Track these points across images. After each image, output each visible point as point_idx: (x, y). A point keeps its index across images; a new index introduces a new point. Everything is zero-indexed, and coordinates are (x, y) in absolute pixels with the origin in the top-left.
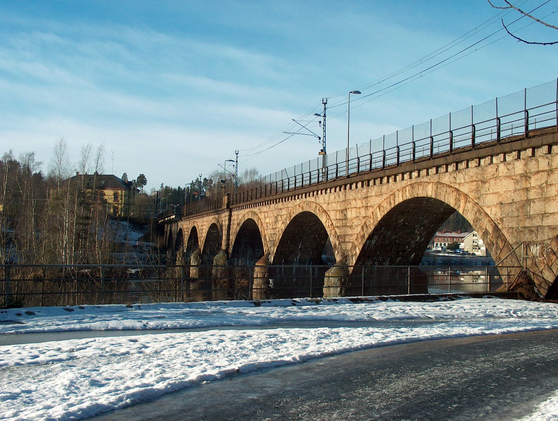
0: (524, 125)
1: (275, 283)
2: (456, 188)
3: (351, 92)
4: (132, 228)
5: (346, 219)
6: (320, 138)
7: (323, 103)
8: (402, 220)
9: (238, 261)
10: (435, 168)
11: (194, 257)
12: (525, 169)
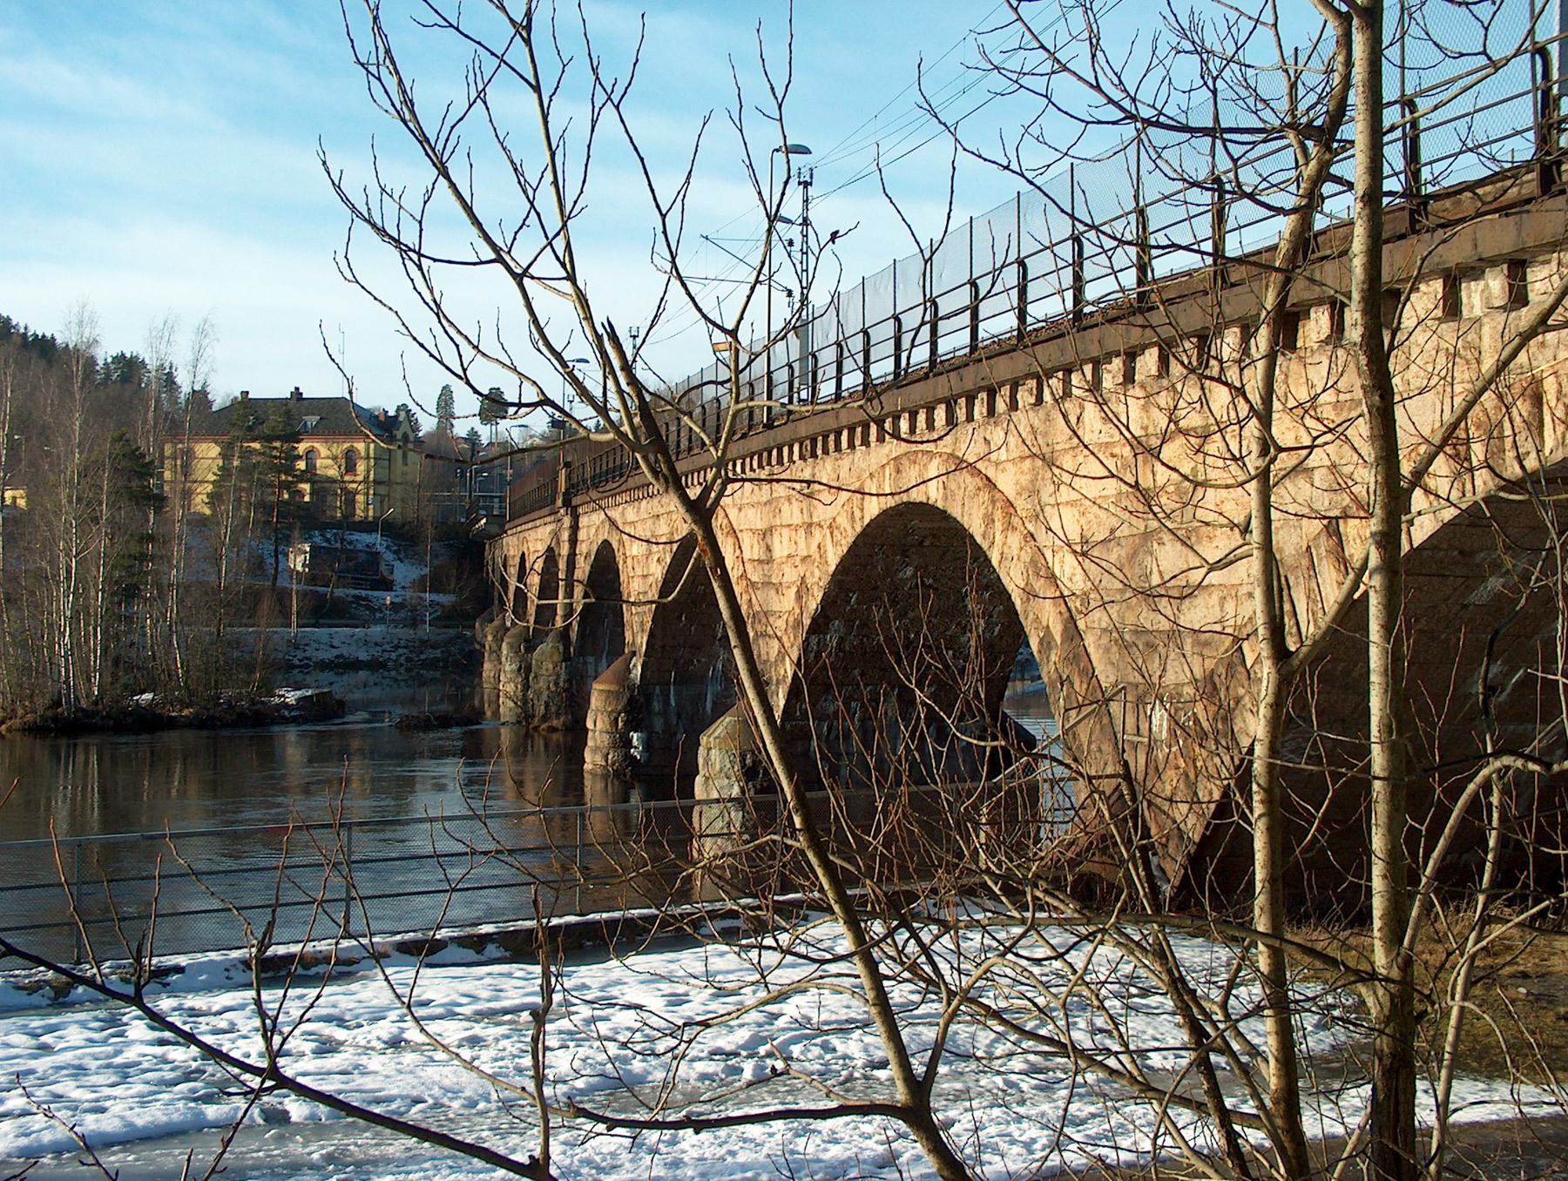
1: (648, 745)
2: (988, 478)
3: (777, 150)
4: (395, 552)
5: (770, 561)
7: (800, 183)
8: (909, 571)
9: (596, 666)
11: (511, 646)
12: (1146, 421)
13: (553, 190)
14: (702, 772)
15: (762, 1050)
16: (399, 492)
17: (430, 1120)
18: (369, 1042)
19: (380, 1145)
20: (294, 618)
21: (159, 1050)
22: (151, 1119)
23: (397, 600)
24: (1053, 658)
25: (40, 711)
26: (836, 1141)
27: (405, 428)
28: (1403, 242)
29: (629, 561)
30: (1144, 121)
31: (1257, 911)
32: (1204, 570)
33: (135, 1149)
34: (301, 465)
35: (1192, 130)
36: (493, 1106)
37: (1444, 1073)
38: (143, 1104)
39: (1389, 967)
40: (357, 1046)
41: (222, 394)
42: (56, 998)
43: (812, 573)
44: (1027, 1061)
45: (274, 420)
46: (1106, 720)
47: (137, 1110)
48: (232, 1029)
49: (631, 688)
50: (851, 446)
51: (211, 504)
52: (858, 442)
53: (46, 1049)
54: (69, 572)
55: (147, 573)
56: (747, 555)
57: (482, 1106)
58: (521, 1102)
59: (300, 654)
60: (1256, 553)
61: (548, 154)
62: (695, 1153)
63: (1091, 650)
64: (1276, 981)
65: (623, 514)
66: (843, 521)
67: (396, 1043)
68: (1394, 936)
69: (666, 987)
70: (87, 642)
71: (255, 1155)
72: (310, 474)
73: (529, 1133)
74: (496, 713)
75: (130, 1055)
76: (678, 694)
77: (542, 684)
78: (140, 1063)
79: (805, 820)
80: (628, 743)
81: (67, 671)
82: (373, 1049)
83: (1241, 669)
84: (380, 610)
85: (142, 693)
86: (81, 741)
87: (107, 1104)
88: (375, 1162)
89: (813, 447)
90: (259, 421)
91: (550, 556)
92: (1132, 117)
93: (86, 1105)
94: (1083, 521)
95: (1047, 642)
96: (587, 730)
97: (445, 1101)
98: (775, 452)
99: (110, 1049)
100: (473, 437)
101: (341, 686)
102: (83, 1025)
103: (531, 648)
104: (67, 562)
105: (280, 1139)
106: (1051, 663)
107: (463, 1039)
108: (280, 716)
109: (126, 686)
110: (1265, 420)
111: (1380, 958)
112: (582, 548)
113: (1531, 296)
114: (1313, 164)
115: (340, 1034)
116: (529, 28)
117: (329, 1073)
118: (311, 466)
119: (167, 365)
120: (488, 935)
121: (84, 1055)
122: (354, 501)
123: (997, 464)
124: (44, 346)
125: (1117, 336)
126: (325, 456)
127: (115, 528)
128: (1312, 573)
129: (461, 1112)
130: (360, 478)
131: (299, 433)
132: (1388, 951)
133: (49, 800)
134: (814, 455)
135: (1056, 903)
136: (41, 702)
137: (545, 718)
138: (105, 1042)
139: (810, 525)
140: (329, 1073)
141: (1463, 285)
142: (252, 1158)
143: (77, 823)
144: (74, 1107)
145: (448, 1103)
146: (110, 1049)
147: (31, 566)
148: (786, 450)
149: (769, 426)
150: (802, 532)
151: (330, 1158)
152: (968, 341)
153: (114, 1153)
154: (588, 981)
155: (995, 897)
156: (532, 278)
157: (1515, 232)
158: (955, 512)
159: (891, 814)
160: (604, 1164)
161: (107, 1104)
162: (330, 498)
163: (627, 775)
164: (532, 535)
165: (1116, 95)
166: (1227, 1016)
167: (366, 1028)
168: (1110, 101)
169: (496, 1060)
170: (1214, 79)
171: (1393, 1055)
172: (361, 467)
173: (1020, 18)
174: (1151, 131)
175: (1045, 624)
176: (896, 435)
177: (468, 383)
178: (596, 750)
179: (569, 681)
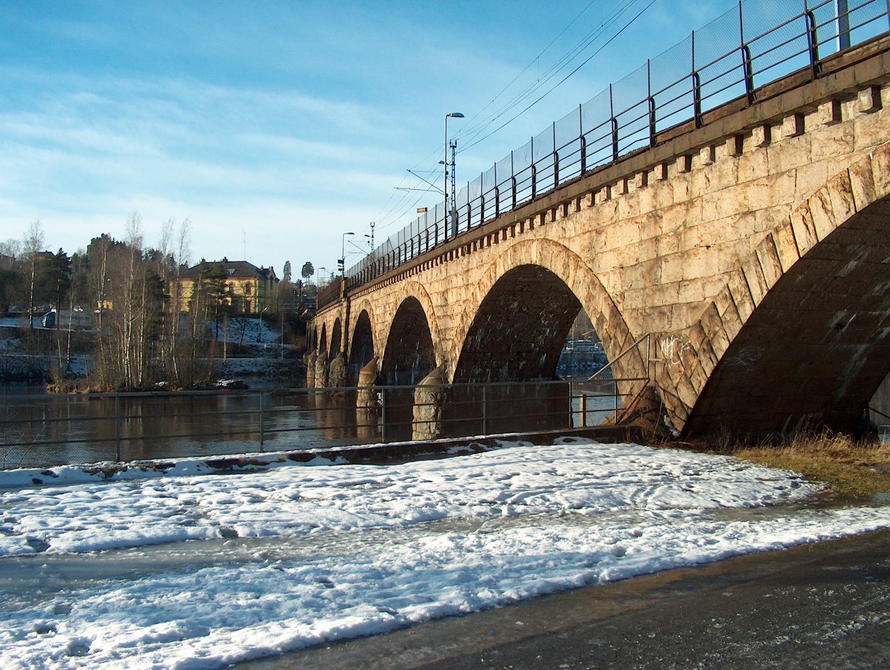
8: (516, 304)
10: (733, 139)
11: (320, 362)
15: (509, 500)
17: (324, 536)
18: (280, 497)
19: (296, 549)
20: (225, 354)
21: (160, 500)
22: (154, 534)
24: (605, 327)
27: (271, 274)
28: (810, 84)
29: (375, 317)
33: (144, 549)
34: (227, 289)
36: (361, 529)
38: (149, 526)
40: (273, 499)
41: (194, 261)
42: (106, 477)
43: (469, 307)
46: (636, 353)
47: (146, 529)
48: (202, 490)
49: (377, 373)
53: (97, 499)
56: (434, 303)
57: (353, 529)
58: (377, 527)
59: (227, 370)
63: (627, 320)
67: (296, 498)
71: (218, 554)
72: (230, 293)
73: (386, 543)
75: (143, 502)
77: (335, 376)
78: (149, 506)
82: (283, 501)
83: (717, 317)
84: (261, 351)
87: (129, 525)
88: (294, 559)
91: (337, 322)
93: (116, 525)
94: (620, 258)
95: (601, 320)
97: (331, 526)
98: (449, 254)
99: (132, 499)
100: (300, 283)
105: (232, 546)
106: (604, 330)
107: (335, 496)
112: (352, 315)
113: (884, 104)
115: (263, 494)
120: (337, 452)
121: (117, 502)
123: (569, 239)
126: (237, 286)
127: (148, 309)
128: (758, 263)
129: (342, 532)
130: (252, 294)
138: (130, 495)
139: (468, 285)
140: (259, 512)
141: (842, 105)
142: (216, 556)
144: (109, 527)
145: (332, 528)
146: (132, 499)
150: (463, 289)
151: (265, 556)
153: (132, 552)
157: (880, 67)
158: (547, 265)
160: (442, 558)
161: (129, 525)
169: (357, 505)
172: (253, 289)
175: (600, 311)
179: (347, 374)
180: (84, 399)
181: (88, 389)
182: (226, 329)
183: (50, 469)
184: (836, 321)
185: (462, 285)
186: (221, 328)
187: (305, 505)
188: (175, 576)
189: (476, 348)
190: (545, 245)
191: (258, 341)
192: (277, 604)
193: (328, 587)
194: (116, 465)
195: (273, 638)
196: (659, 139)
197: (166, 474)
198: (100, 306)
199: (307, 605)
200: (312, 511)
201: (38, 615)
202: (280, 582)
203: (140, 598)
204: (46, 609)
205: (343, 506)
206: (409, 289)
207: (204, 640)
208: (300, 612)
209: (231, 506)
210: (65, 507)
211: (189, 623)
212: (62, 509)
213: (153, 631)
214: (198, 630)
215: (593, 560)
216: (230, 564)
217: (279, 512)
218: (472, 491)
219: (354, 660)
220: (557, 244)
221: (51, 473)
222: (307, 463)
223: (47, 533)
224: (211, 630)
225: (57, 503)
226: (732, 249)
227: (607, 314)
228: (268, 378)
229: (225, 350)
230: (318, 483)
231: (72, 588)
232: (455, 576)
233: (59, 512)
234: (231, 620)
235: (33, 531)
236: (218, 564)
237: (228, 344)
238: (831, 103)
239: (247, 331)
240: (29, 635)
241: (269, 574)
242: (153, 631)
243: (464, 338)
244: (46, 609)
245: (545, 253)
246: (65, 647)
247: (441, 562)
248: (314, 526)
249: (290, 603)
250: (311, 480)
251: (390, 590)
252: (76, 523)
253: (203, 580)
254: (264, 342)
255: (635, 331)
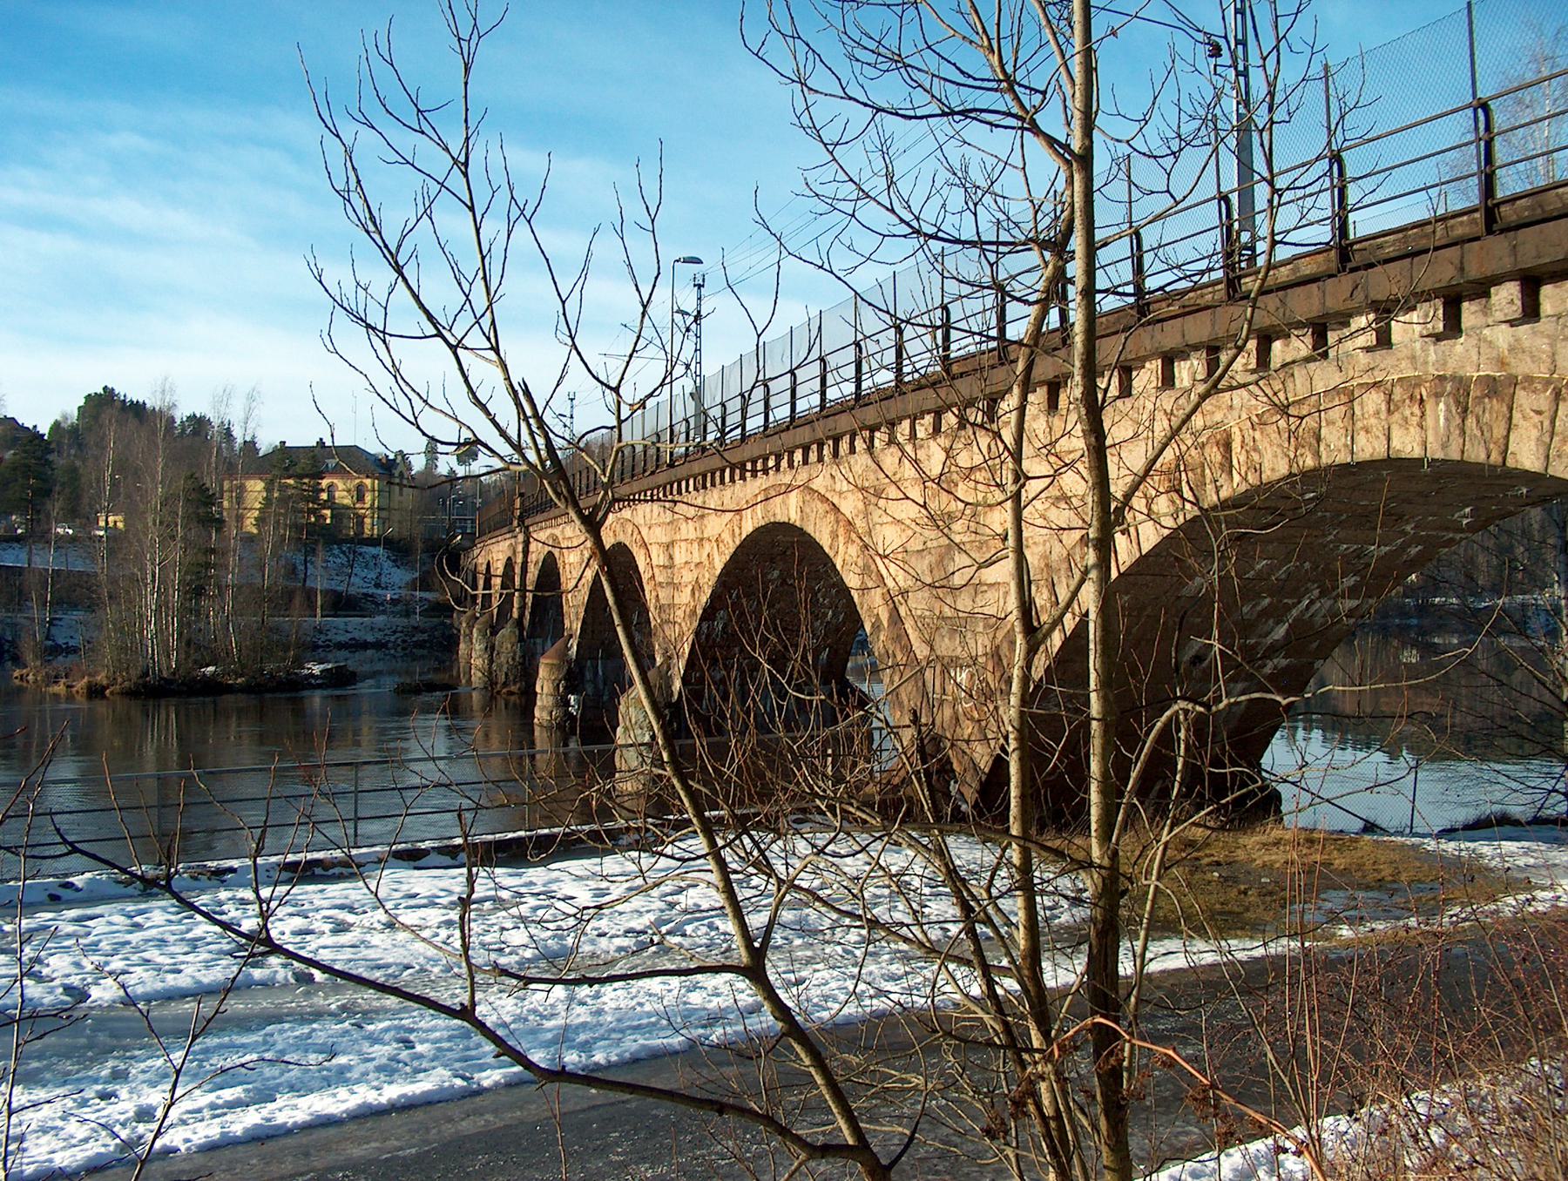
0: (1475, 168)
1: (584, 706)
4: (394, 561)
5: (672, 566)
6: (1216, 51)
8: (776, 573)
10: (1045, 389)
11: (479, 630)
13: (483, 283)
14: (622, 724)
15: (664, 929)
16: (396, 516)
20: (319, 611)
23: (396, 597)
25: (134, 679)
26: (718, 995)
27: (401, 468)
30: (926, 235)
31: (1011, 819)
32: (975, 568)
34: (324, 496)
35: (964, 243)
37: (1142, 934)
38: (207, 968)
39: (1102, 857)
40: (363, 927)
41: (266, 444)
42: (145, 890)
44: (860, 935)
45: (304, 462)
49: (569, 662)
50: (732, 480)
51: (257, 525)
52: (737, 477)
53: (138, 927)
54: (154, 576)
55: (211, 577)
56: (655, 562)
59: (323, 638)
60: (1011, 555)
61: (479, 256)
62: (613, 1005)
63: (910, 631)
64: (1026, 869)
65: (563, 532)
66: (726, 536)
68: (1106, 836)
69: (593, 884)
70: (167, 628)
72: (331, 503)
74: (469, 681)
76: (604, 667)
79: (671, 754)
80: (567, 704)
81: (153, 650)
84: (382, 604)
85: (207, 666)
86: (163, 702)
87: (182, 967)
88: (377, 1011)
89: (704, 481)
90: (293, 464)
91: (509, 564)
92: (918, 232)
95: (877, 626)
96: (536, 694)
97: (428, 967)
98: (675, 485)
101: (353, 662)
102: (164, 909)
103: (494, 633)
104: (152, 569)
105: (307, 994)
108: (308, 683)
109: (195, 662)
110: (1017, 457)
111: (1096, 852)
112: (532, 557)
114: (1050, 267)
115: (350, 918)
116: (466, 164)
117: (342, 947)
118: (331, 497)
119: (226, 422)
121: (165, 932)
122: (363, 522)
124: (138, 409)
125: (929, 398)
126: (341, 489)
130: (367, 506)
131: (322, 472)
132: (1101, 846)
133: (141, 747)
134: (704, 487)
135: (864, 816)
136: (135, 673)
137: (505, 684)
138: (179, 922)
139: (702, 539)
140: (342, 947)
143: (162, 761)
144: (159, 969)
147: (127, 573)
148: (684, 484)
149: (671, 465)
150: (696, 545)
151: (343, 1008)
152: (818, 403)
153: (188, 1002)
154: (534, 879)
155: (822, 813)
156: (466, 348)
158: (810, 529)
159: (738, 751)
161: (182, 967)
162: (345, 521)
163: (564, 727)
164: (495, 548)
165: (908, 217)
166: (990, 897)
167: (370, 914)
168: (902, 220)
170: (976, 205)
171: (1104, 921)
172: (368, 497)
173: (834, 159)
174: (931, 242)
176: (766, 471)
177: (418, 427)
178: (543, 708)
179: (523, 657)
180: (78, 698)
181: (86, 680)
182: (319, 563)
183: (71, 879)
184: (1192, 653)
185: (694, 537)
186: (312, 563)
187: (402, 936)
188: (239, 1034)
189: (714, 640)
190: (808, 498)
191: (377, 586)
192: (348, 1068)
193: (407, 1048)
194: (157, 872)
195: (339, 1104)
196: (955, 369)
197: (224, 884)
198: (102, 524)
199: (379, 1069)
200: (408, 945)
201: (96, 1081)
202: (355, 1041)
203: (202, 1061)
204: (103, 1073)
205: (449, 938)
206: (618, 530)
207: (270, 1106)
208: (372, 1076)
209: (308, 938)
210: (100, 941)
211: (255, 1088)
212: (96, 944)
213: (218, 1097)
214: (265, 1096)
215: (714, 1019)
216: (304, 1018)
217: (367, 947)
218: (621, 914)
219: (416, 1127)
220: (823, 499)
221: (72, 884)
222: (417, 863)
223: (84, 979)
224: (278, 1096)
225: (89, 934)
226: (1041, 548)
227: (884, 617)
228: (392, 651)
229: (319, 603)
230: (424, 901)
231: (126, 1048)
232: (549, 1036)
233: (94, 947)
234: (299, 1085)
235: (68, 976)
236: (289, 1018)
237: (325, 593)
238: (1160, 361)
239: (357, 570)
240: (91, 1102)
241: (346, 1032)
242: (218, 1097)
243: (696, 624)
244: (103, 1073)
245: (807, 510)
246: (131, 1114)
247: (543, 1017)
248: (408, 967)
249: (362, 1067)
250: (414, 896)
251: (473, 1053)
252: (117, 964)
253: (270, 1040)
254: (386, 588)
255: (921, 651)
